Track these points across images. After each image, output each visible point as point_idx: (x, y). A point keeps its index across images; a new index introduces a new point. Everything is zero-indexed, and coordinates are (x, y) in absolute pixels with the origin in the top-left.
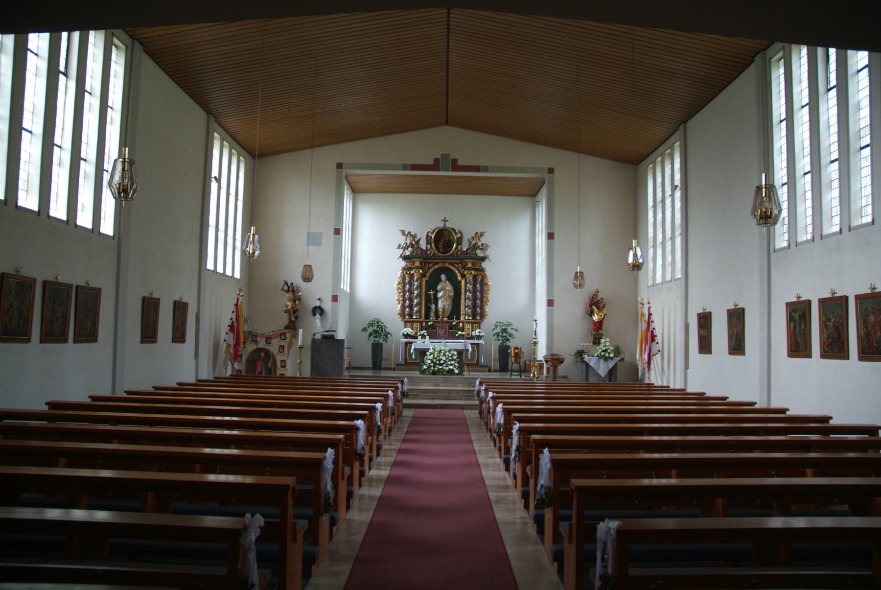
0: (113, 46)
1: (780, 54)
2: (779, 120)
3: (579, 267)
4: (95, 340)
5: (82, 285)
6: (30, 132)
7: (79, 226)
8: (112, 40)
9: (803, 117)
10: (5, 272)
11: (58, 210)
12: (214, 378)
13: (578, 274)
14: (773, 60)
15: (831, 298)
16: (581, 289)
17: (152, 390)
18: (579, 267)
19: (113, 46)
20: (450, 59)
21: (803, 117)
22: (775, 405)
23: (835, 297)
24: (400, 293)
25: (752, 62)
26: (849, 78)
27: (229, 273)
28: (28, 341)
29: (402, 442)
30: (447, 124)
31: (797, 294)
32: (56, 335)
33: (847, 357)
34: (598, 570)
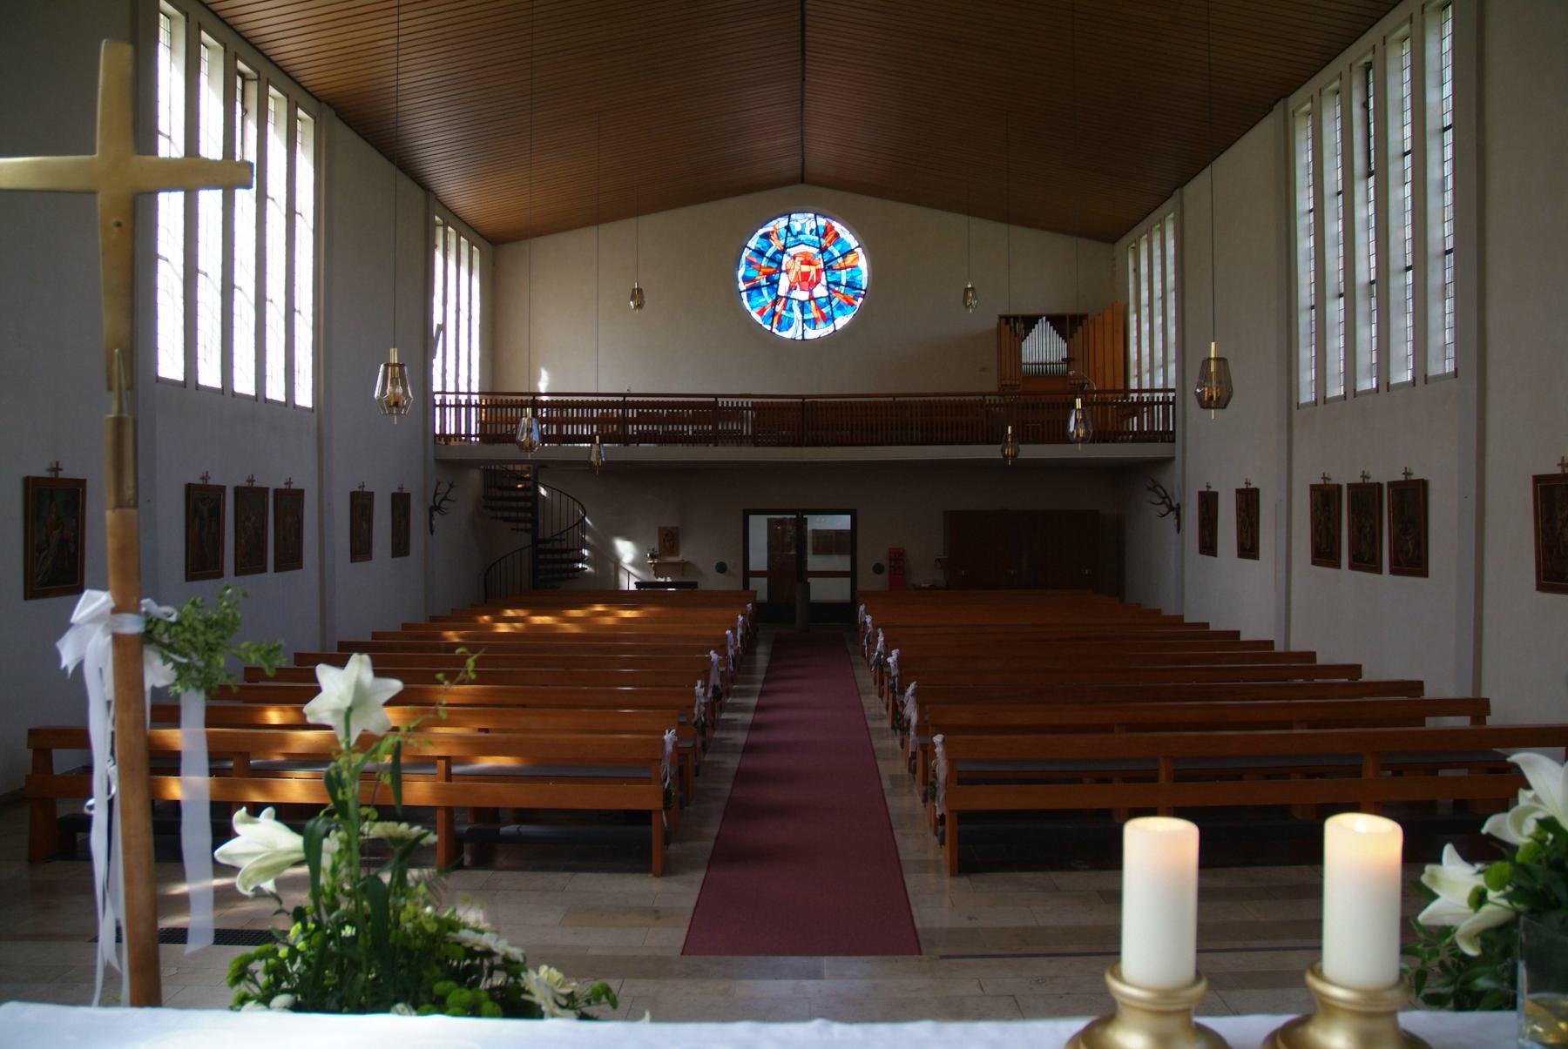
0: (202, 46)
1: (1405, 29)
2: (1400, 152)
3: (1213, 344)
4: (300, 566)
5: (243, 485)
6: (167, 260)
7: (202, 386)
8: (236, 64)
9: (1334, 207)
10: (192, 482)
11: (209, 376)
12: (375, 635)
13: (1212, 363)
14: (1167, 219)
15: (1360, 484)
16: (1220, 411)
17: (369, 639)
18: (1213, 344)
19: (202, 46)
20: (807, 34)
21: (1334, 207)
22: (1297, 646)
23: (1368, 484)
24: (728, 442)
25: (1171, 196)
26: (1390, 161)
27: (275, 391)
28: (220, 575)
29: (743, 752)
30: (803, 181)
31: (1406, 468)
32: (1365, 560)
33: (1380, 572)
34: (910, 751)
